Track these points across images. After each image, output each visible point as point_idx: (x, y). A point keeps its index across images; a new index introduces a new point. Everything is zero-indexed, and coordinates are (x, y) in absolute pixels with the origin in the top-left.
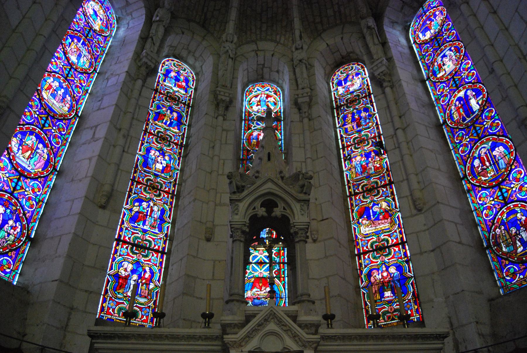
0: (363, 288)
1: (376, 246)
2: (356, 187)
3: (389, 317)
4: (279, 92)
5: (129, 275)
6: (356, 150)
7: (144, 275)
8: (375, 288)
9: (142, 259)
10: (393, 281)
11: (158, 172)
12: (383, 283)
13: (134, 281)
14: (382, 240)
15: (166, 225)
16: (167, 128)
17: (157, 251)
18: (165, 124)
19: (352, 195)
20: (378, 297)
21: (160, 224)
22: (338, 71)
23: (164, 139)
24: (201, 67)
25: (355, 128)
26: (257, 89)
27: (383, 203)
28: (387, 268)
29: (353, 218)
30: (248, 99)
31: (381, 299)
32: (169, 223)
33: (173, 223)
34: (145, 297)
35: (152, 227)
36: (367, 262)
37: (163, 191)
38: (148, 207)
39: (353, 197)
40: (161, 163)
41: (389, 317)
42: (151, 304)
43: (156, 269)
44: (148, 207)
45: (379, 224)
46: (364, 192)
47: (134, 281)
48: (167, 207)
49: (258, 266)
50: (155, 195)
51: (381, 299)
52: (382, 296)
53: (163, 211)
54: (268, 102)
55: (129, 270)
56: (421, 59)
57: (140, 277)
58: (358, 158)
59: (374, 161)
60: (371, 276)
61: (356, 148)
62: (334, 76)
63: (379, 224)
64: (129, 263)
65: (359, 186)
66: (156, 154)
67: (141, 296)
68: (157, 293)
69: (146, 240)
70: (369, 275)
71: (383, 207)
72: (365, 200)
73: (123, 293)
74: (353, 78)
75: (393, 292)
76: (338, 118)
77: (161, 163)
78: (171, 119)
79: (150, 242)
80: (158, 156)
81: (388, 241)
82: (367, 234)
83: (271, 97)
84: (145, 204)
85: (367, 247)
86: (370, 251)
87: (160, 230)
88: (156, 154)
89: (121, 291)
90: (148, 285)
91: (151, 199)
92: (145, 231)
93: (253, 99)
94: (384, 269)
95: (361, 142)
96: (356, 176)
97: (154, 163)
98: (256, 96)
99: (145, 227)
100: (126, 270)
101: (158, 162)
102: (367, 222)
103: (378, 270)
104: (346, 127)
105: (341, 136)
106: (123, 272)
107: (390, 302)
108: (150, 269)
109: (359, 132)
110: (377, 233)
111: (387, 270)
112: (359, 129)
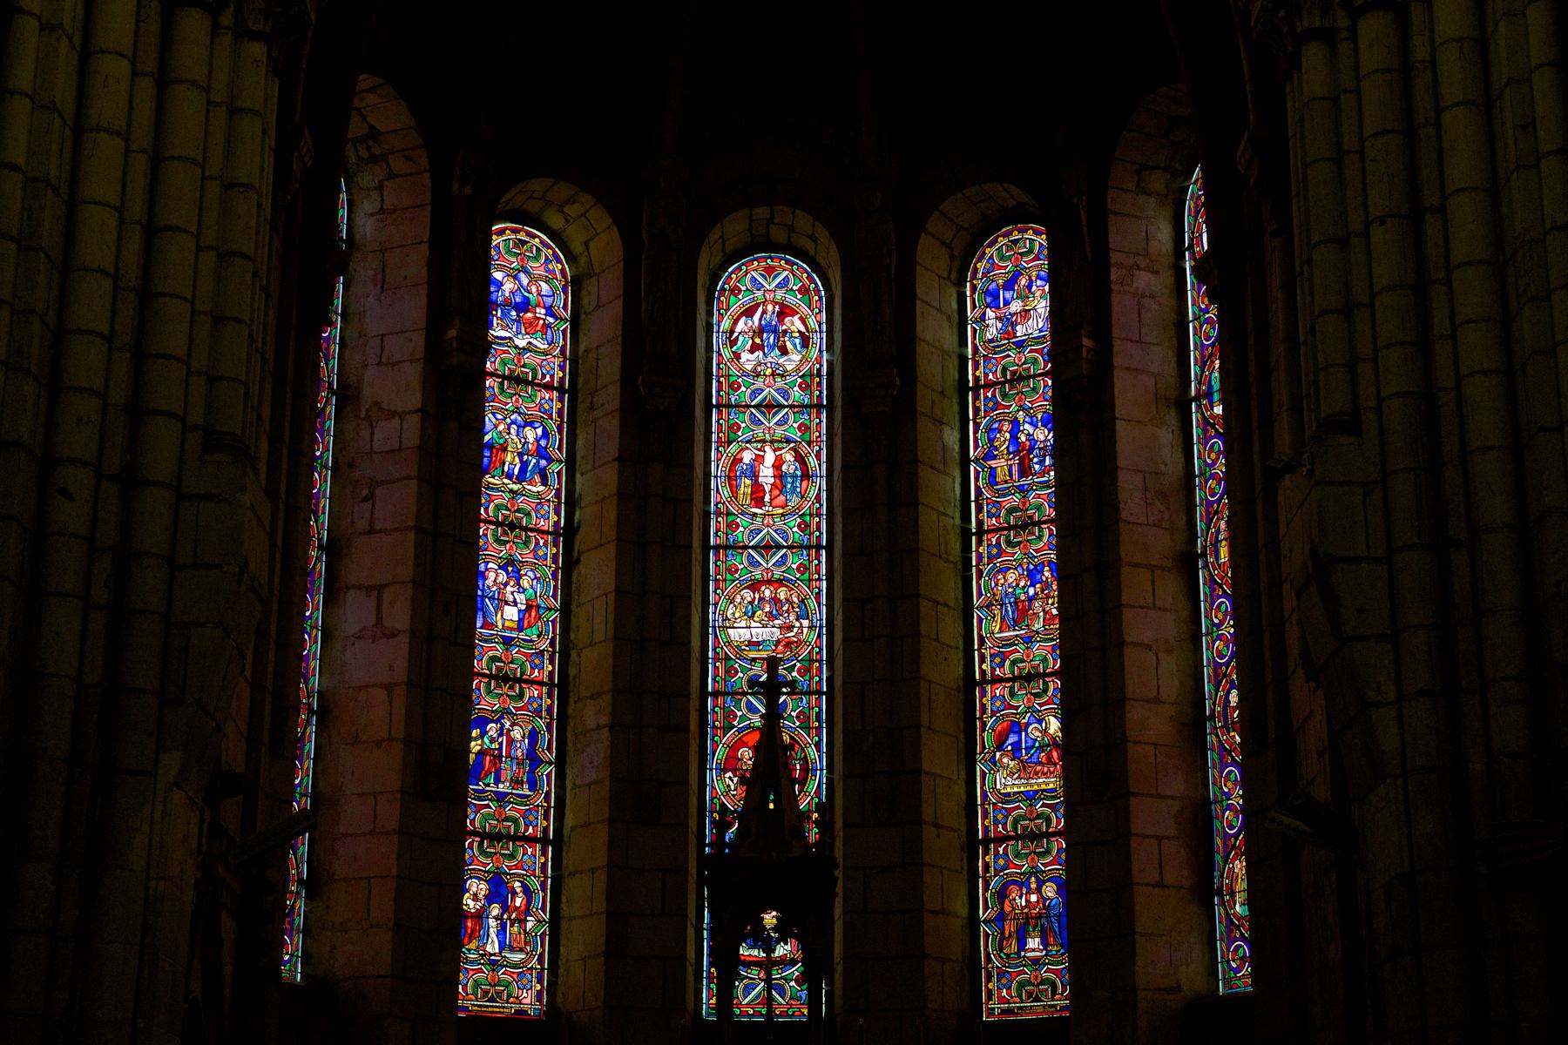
0: (985, 922)
1: (1024, 828)
2: (997, 660)
3: (1029, 994)
4: (817, 291)
5: (483, 907)
6: (1009, 550)
7: (513, 900)
8: (1010, 927)
9: (506, 865)
10: (1048, 917)
11: (511, 629)
12: (1027, 917)
13: (496, 918)
14: (1038, 817)
15: (546, 770)
16: (515, 487)
17: (532, 840)
18: (509, 476)
19: (988, 682)
20: (1014, 947)
21: (532, 771)
22: (990, 246)
23: (512, 527)
24: (586, 244)
25: (1016, 477)
26: (754, 279)
27: (1052, 719)
28: (1040, 883)
29: (984, 747)
30: (726, 324)
31: (1018, 953)
32: (550, 763)
33: (560, 764)
34: (521, 950)
35: (516, 782)
36: (1001, 862)
37: (527, 682)
38: (501, 735)
39: (988, 688)
40: (515, 603)
41: (1029, 994)
42: (534, 963)
43: (535, 884)
44: (501, 735)
45: (1036, 773)
46: (1013, 679)
47: (496, 918)
48: (541, 724)
49: (763, 414)
50: (500, 660)
51: (1018, 953)
52: (1022, 945)
53: (533, 736)
54: (785, 332)
55: (481, 895)
56: (1196, 318)
57: (505, 908)
58: (1012, 576)
59: (1048, 597)
60: (1006, 897)
61: (1009, 543)
62: (979, 260)
63: (1036, 773)
64: (479, 879)
65: (1003, 661)
66: (500, 579)
67: (512, 950)
68: (543, 936)
69: (507, 819)
70: (1002, 895)
71: (1051, 731)
72: (1013, 703)
73: (477, 949)
74: (1029, 287)
75: (1045, 943)
76: (977, 426)
77: (515, 603)
78: (520, 455)
79: (515, 821)
80: (506, 584)
81: (1048, 820)
82: (1008, 794)
83: (794, 313)
84: (492, 728)
85: (1004, 827)
86: (1010, 838)
87: (533, 786)
88: (500, 579)
89: (473, 945)
90: (523, 922)
91: (505, 712)
92: (501, 798)
93: (740, 326)
94: (1033, 886)
95: (1024, 527)
96: (1001, 630)
97: (499, 608)
98: (749, 313)
99: (502, 788)
100: (475, 898)
101: (507, 603)
102: (1012, 763)
103: (1020, 885)
104: (993, 463)
105: (979, 492)
106: (471, 903)
107: (1036, 962)
108: (524, 886)
109: (1023, 490)
110: (1031, 797)
111: (1039, 890)
112: (1025, 481)
